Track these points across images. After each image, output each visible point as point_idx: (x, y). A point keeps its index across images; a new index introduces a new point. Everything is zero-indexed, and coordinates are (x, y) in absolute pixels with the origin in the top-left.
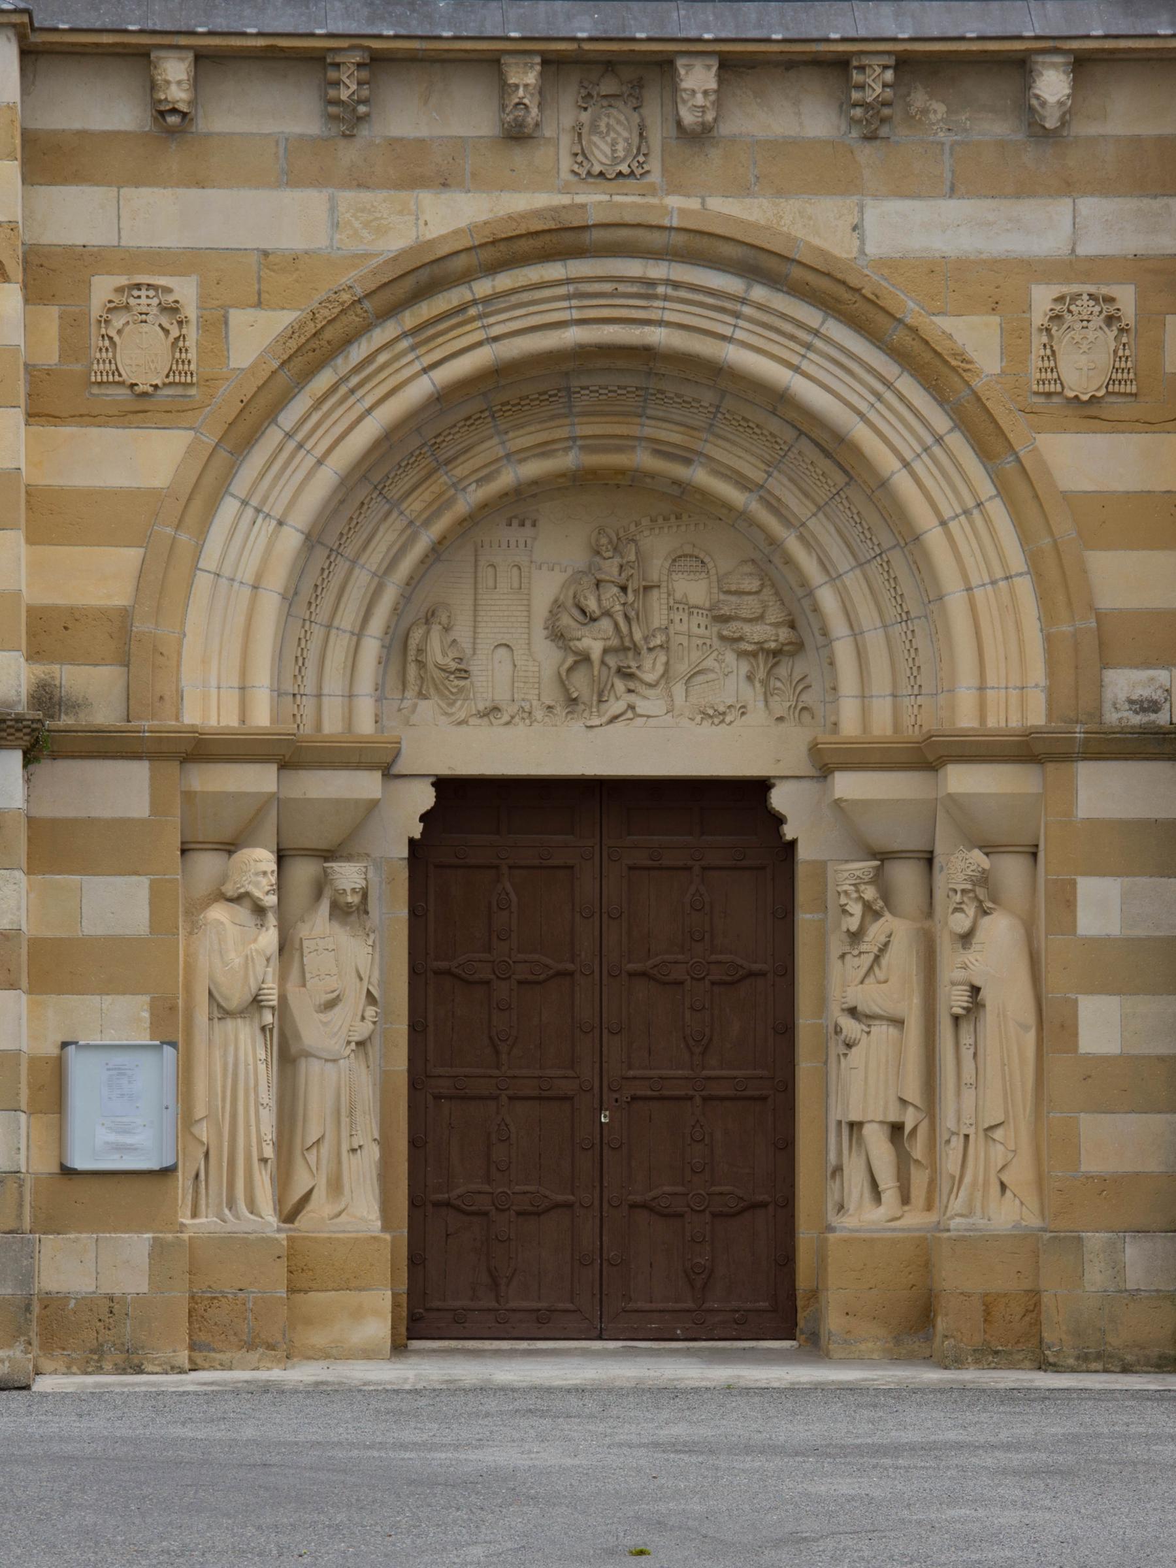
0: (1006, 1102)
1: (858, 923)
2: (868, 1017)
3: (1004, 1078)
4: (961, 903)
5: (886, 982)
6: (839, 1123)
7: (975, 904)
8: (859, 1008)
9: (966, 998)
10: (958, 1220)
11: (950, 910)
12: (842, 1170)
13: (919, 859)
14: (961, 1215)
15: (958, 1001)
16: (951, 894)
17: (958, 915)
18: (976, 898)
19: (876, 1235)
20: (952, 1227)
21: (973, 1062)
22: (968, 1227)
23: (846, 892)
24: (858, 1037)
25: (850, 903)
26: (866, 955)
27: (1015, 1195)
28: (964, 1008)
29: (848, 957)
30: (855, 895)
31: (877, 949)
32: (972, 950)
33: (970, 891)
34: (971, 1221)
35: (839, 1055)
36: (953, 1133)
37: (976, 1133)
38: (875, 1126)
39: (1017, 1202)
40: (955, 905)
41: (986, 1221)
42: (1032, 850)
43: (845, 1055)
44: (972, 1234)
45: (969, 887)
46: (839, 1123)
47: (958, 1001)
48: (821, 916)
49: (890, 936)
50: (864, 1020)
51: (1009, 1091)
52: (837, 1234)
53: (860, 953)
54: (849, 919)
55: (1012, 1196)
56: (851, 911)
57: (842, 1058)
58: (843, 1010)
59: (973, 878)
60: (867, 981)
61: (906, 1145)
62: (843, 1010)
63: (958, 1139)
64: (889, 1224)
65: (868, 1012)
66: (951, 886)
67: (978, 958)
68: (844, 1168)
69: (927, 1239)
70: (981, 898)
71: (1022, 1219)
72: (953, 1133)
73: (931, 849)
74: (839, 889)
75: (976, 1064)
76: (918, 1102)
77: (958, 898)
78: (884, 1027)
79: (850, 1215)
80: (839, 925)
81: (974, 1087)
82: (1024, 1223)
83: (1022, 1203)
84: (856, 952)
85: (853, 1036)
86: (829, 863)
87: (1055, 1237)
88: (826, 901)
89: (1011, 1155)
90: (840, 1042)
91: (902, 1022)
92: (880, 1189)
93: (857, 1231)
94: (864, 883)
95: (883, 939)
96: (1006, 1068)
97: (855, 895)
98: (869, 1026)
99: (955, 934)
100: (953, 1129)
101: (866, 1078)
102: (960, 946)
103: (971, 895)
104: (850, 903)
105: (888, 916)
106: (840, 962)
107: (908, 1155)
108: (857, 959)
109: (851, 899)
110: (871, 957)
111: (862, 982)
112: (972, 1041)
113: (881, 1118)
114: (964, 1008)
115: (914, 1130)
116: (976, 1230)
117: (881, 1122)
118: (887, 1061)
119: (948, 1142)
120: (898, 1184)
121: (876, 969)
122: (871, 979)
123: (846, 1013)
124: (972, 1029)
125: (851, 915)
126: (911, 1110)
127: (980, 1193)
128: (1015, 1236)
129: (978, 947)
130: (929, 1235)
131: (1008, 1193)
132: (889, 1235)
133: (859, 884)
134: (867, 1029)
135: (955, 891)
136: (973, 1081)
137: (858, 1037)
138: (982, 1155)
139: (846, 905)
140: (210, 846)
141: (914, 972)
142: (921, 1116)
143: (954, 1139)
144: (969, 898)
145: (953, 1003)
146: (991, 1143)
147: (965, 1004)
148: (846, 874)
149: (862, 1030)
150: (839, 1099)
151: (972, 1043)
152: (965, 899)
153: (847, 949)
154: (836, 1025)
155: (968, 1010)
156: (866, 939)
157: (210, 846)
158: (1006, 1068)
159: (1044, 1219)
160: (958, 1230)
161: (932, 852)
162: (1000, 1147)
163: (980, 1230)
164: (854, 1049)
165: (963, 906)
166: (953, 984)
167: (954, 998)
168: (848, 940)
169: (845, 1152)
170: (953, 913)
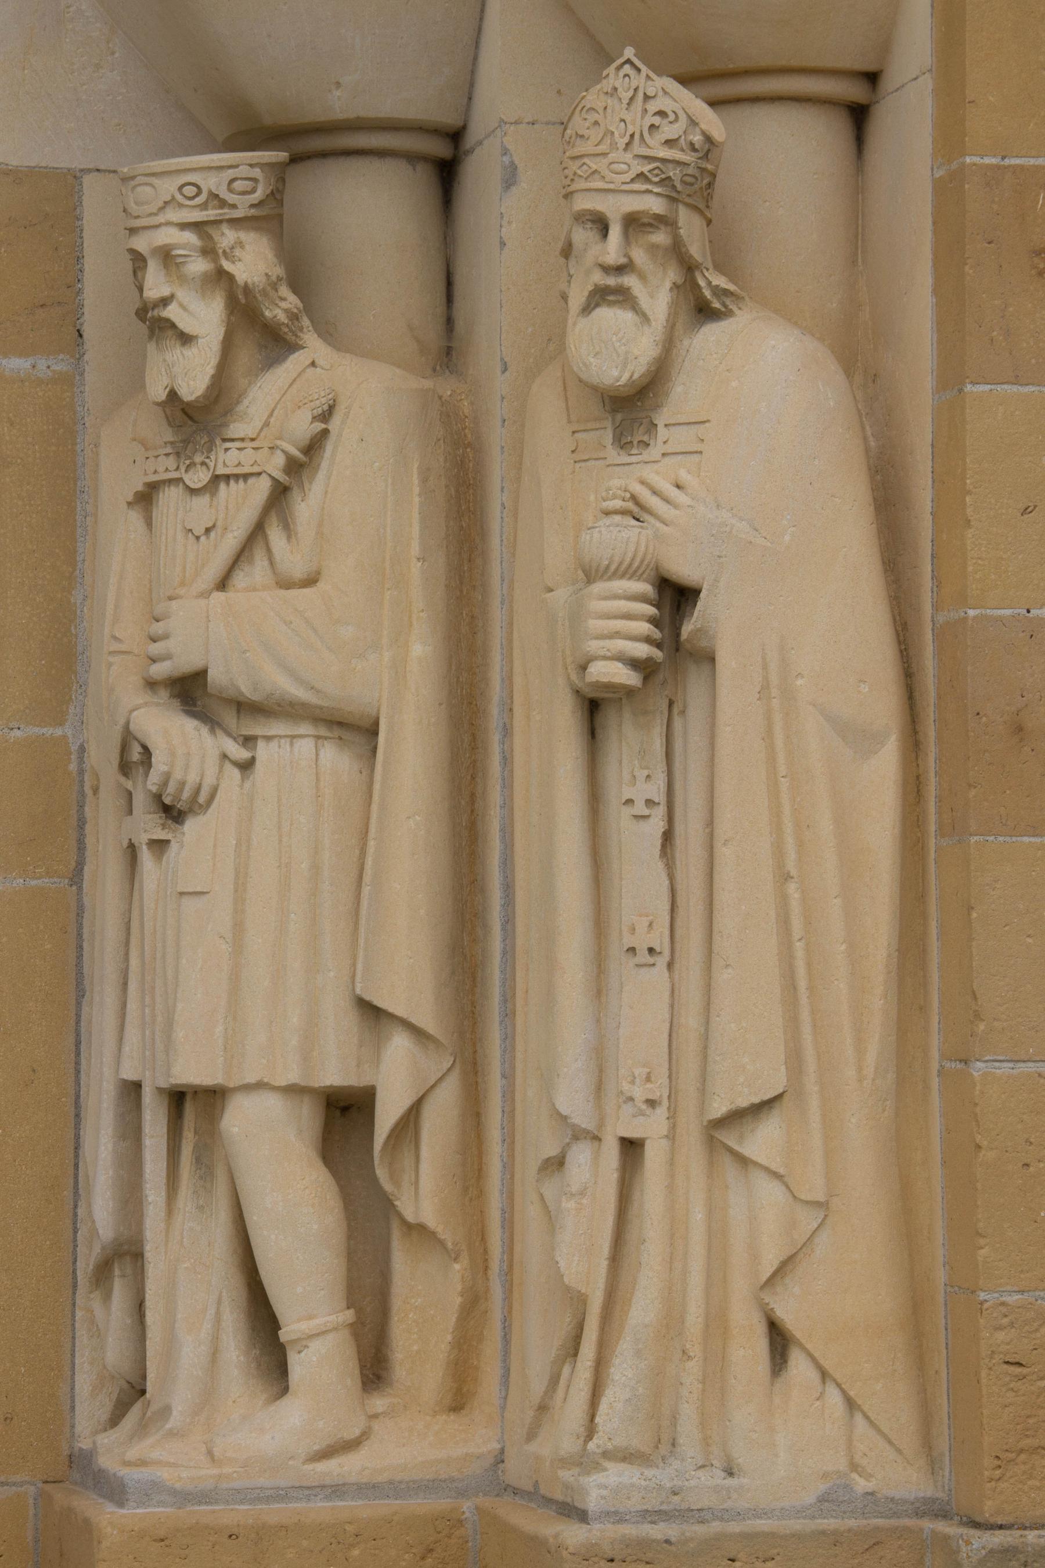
0: (792, 1022)
1: (210, 370)
2: (245, 707)
3: (784, 922)
4: (620, 270)
5: (310, 581)
6: (132, 1090)
7: (673, 275)
8: (216, 676)
9: (644, 628)
10: (616, 1474)
11: (577, 297)
12: (137, 1256)
13: (412, 158)
14: (628, 1456)
15: (617, 635)
16: (582, 236)
17: (608, 316)
18: (678, 253)
19: (274, 1513)
20: (593, 1502)
21: (660, 866)
22: (653, 1504)
23: (166, 256)
24: (209, 781)
25: (181, 294)
26: (236, 488)
27: (824, 1375)
28: (635, 664)
29: (169, 499)
30: (198, 266)
31: (280, 460)
32: (654, 452)
33: (660, 221)
34: (663, 1476)
35: (132, 850)
36: (578, 1135)
37: (671, 1136)
38: (272, 1104)
39: (834, 1397)
40: (598, 278)
41: (718, 1477)
42: (854, 91)
43: (159, 846)
44: (670, 1530)
45: (655, 205)
46: (132, 1090)
47: (617, 635)
48: (60, 365)
49: (326, 416)
50: (229, 718)
51: (802, 984)
52: (132, 1513)
53: (216, 479)
54: (177, 355)
55: (814, 1375)
56: (184, 323)
57: (146, 856)
58: (151, 685)
59: (674, 173)
60: (240, 579)
61: (381, 1173)
62: (151, 685)
63: (596, 1156)
64: (322, 1467)
65: (247, 690)
66: (584, 203)
67: (684, 476)
68: (148, 1255)
69: (460, 1523)
70: (696, 250)
71: (854, 1467)
72: (578, 1135)
73: (450, 119)
74: (142, 244)
75: (671, 877)
76: (426, 1019)
77: (613, 249)
78: (305, 747)
79: (172, 1434)
80: (137, 383)
81: (662, 961)
82: (861, 1485)
83: (851, 1404)
84: (199, 478)
85: (192, 778)
86: (87, 180)
87: (1008, 1552)
88: (77, 311)
89: (808, 1220)
90: (140, 800)
91: (372, 731)
92: (284, 1335)
93: (204, 1497)
94: (234, 222)
95: (303, 427)
96: (792, 888)
97: (198, 266)
98: (249, 741)
99: (595, 388)
100: (583, 1119)
101: (239, 928)
102: (608, 437)
103: (660, 237)
104: (181, 294)
105: (314, 346)
106: (135, 517)
107: (388, 1204)
108: (203, 500)
109: (183, 279)
110: (262, 488)
111: (223, 584)
112: (656, 789)
113: (292, 1076)
114: (635, 664)
115: (410, 1120)
116: (683, 1515)
117: (293, 1090)
118: (316, 869)
119: (557, 1163)
120: (349, 1315)
121: (275, 535)
122: (257, 571)
123: (164, 694)
124: (658, 745)
125: (186, 339)
126: (399, 1043)
127: (694, 1367)
128: (835, 1539)
129: (681, 438)
130: (467, 1506)
131: (798, 1365)
132: (321, 1510)
133: (217, 223)
134: (242, 754)
135: (602, 225)
136: (659, 938)
137: (209, 781)
138: (698, 1215)
139: (165, 302)
140: (691, 1021)
141: (415, 548)
142: (437, 1064)
143: (580, 1156)
144: (653, 248)
145: (594, 646)
146: (730, 1170)
147: (642, 650)
148: (168, 187)
149: (225, 756)
150: (132, 1006)
151: (660, 798)
152: (639, 256)
153: (165, 467)
154: (128, 738)
155: (644, 667)
156: (236, 429)
157: (691, 1021)
158: (792, 888)
159: (933, 1465)
160: (618, 1517)
161: (456, 136)
162: (770, 1192)
163: (700, 1515)
164: (191, 825)
165: (630, 281)
166: (591, 574)
167: (596, 625)
168: (169, 435)
169: (154, 1194)
170: (587, 309)
